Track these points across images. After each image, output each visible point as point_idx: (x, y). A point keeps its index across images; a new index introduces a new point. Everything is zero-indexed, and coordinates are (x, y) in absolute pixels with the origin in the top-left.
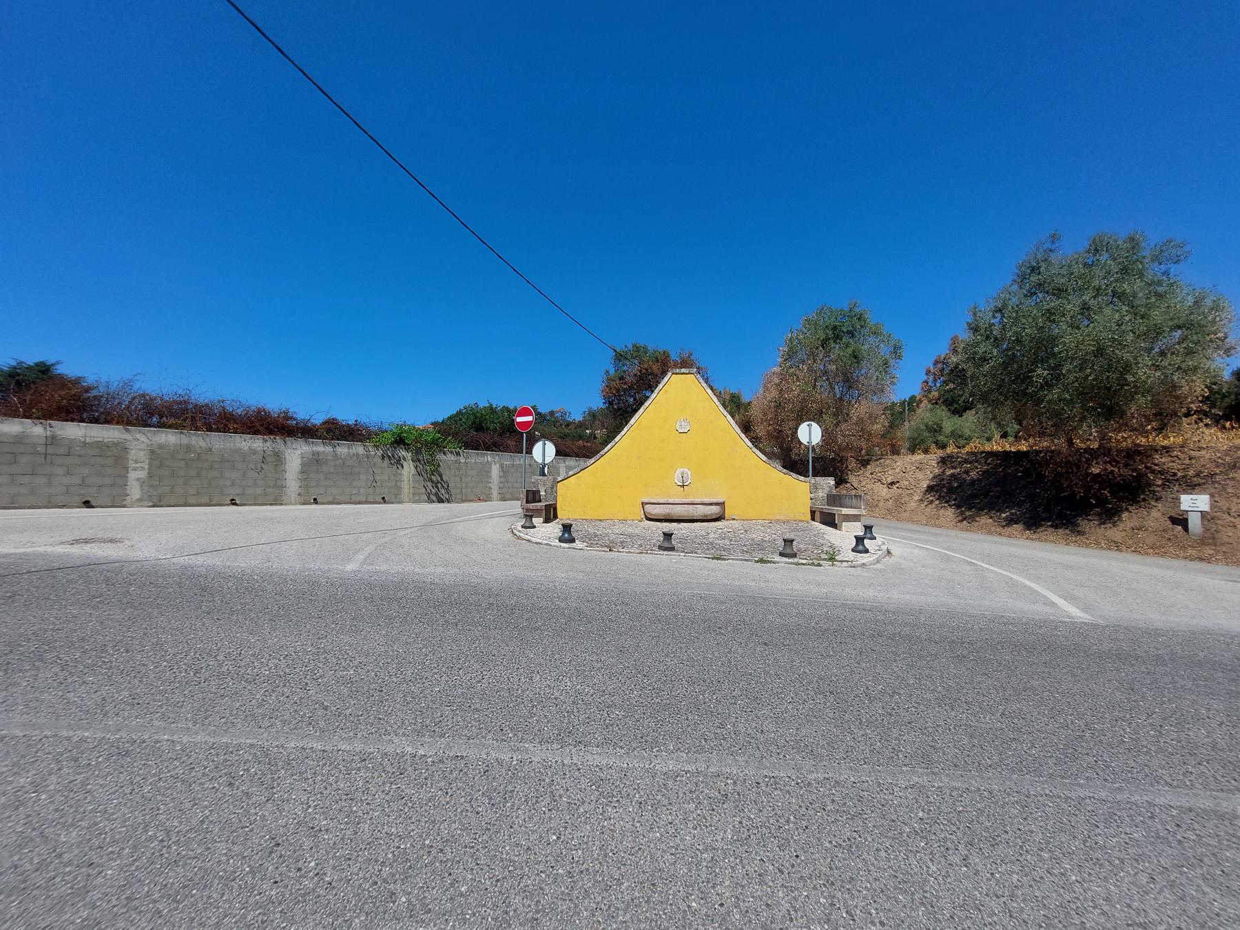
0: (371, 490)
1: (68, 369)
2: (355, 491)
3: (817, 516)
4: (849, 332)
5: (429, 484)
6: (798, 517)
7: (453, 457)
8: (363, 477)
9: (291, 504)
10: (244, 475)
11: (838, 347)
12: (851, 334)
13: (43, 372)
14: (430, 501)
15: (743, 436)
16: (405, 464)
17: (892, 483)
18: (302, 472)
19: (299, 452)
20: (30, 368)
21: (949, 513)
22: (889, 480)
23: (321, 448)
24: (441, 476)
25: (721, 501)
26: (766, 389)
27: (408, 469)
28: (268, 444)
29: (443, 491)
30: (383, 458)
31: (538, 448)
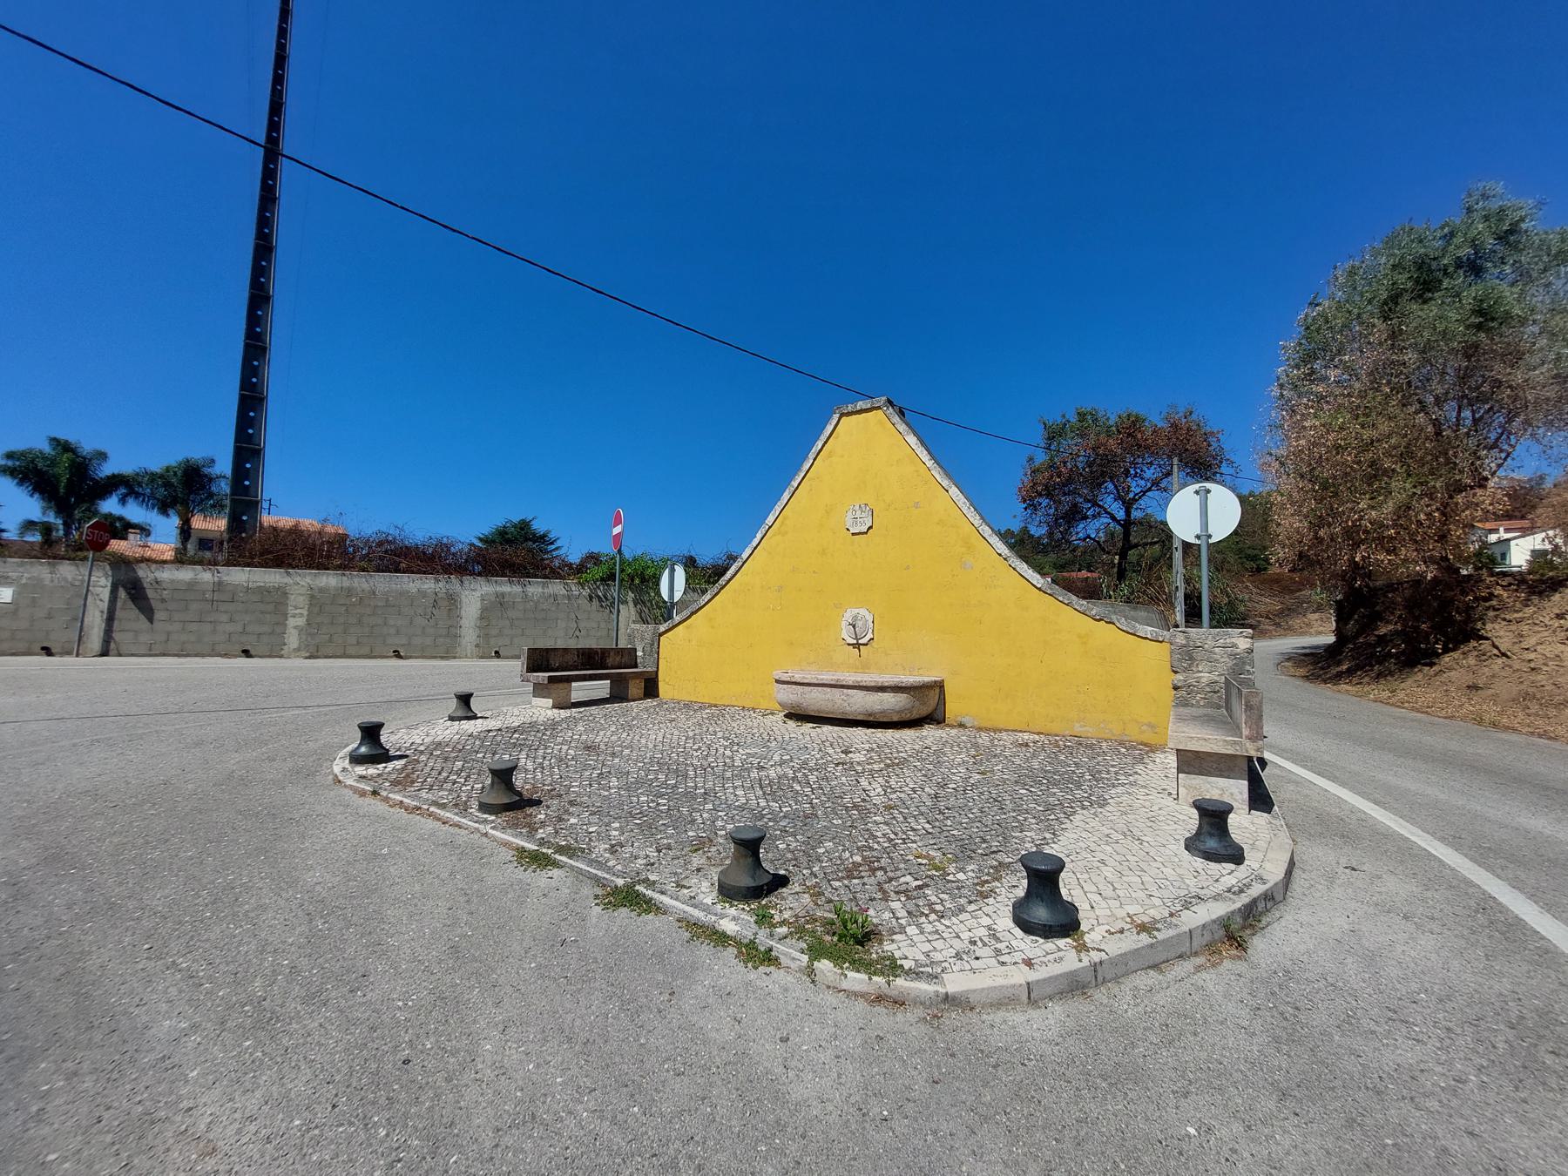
8: (562, 624)
18: (481, 618)
20: (515, 526)
30: (591, 598)
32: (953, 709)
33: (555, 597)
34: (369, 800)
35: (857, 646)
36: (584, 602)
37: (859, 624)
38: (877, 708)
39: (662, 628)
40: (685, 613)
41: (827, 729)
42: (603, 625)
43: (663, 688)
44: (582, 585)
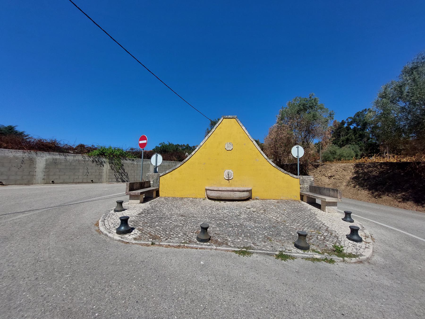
0: (85, 177)
1: (19, 129)
2: (77, 177)
3: (305, 198)
4: (310, 107)
5: (117, 174)
6: (293, 198)
7: (130, 162)
8: (81, 171)
9: (38, 184)
10: (9, 170)
11: (303, 118)
12: (311, 107)
13: (10, 130)
14: (117, 181)
15: (262, 152)
16: (105, 164)
17: (331, 177)
18: (46, 168)
19: (44, 158)
20: (6, 128)
21: (365, 193)
22: (329, 175)
23: (57, 156)
24: (124, 170)
25: (249, 189)
26: (270, 134)
27: (107, 167)
28: (26, 154)
29: (125, 177)
30: (93, 161)
31: (154, 157)
32: (253, 196)
33: (79, 161)
34: (152, 248)
35: (228, 180)
36: (90, 163)
37: (230, 174)
38: (243, 196)
39: (161, 175)
40: (170, 170)
41: (222, 202)
42: (97, 171)
43: (161, 193)
44: (90, 157)
